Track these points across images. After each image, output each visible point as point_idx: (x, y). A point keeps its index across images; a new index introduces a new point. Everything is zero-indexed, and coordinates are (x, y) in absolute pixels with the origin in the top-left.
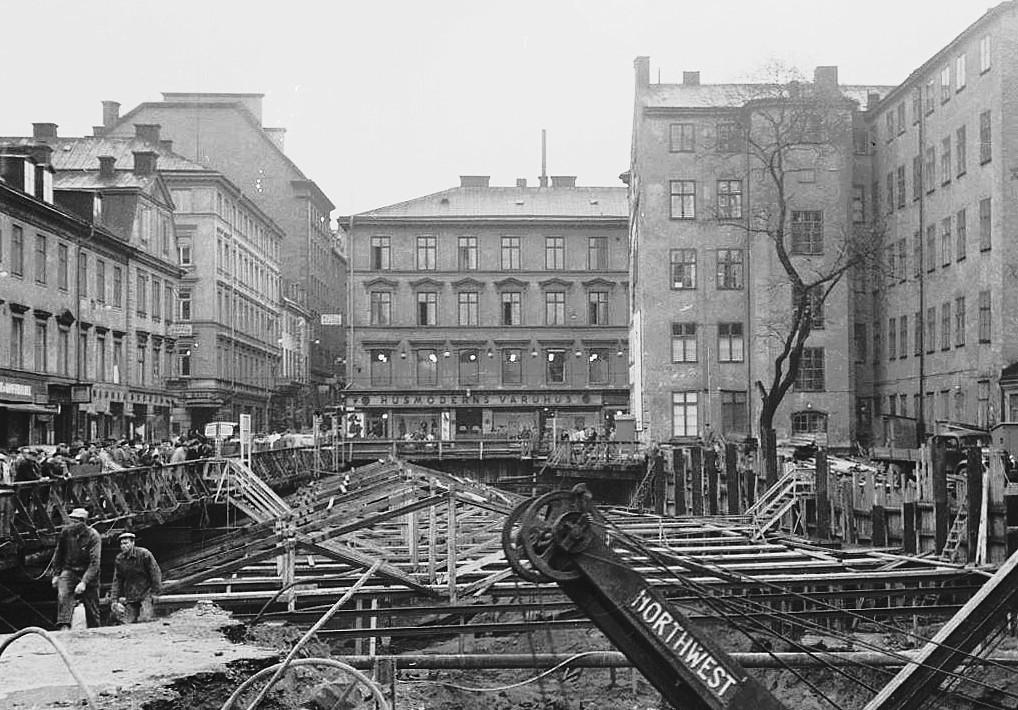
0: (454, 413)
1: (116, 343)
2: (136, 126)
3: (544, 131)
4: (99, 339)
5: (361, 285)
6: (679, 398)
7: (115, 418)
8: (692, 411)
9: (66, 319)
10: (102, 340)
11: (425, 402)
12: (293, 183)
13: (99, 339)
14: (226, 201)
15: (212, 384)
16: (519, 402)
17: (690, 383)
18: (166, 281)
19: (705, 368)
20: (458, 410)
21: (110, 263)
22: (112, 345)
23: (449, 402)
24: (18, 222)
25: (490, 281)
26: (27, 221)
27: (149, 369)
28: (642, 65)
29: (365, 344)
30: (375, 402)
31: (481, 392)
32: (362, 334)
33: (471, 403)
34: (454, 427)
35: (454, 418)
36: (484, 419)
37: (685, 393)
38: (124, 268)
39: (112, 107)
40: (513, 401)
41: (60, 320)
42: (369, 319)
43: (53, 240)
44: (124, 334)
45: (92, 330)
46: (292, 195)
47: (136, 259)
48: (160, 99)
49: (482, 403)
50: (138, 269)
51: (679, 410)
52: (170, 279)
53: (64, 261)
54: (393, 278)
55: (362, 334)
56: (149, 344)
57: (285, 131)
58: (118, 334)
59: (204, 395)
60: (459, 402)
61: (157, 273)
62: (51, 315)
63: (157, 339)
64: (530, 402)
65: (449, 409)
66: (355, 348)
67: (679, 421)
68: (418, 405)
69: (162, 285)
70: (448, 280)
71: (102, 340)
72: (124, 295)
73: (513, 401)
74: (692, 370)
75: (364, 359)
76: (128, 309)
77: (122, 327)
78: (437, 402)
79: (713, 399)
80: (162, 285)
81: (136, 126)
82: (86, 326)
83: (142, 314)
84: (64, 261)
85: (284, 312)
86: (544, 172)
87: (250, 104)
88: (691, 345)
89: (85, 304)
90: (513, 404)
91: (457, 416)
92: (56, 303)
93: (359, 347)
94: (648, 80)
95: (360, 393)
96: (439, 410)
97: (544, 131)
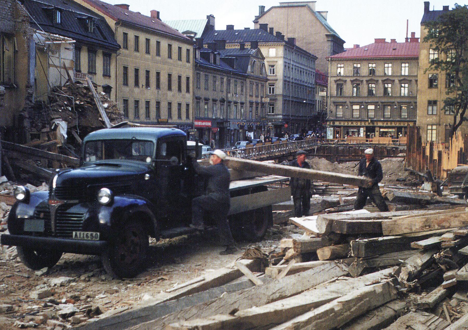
0: (365, 128)
1: (241, 106)
2: (260, 24)
3: (408, 20)
4: (235, 105)
5: (333, 81)
6: (430, 127)
7: (240, 131)
8: (434, 132)
9: (223, 101)
10: (236, 106)
11: (354, 124)
12: (327, 35)
13: (235, 105)
14: (289, 51)
15: (281, 117)
16: (389, 124)
17: (434, 122)
18: (261, 83)
19: (440, 116)
20: (367, 127)
21: (239, 81)
22: (240, 107)
23: (363, 124)
24: (207, 74)
25: (380, 80)
26: (209, 73)
27: (254, 114)
28: (427, 5)
29: (334, 103)
30: (337, 123)
31: (375, 121)
32: (333, 99)
33: (371, 125)
34: (365, 133)
35: (365, 130)
36: (376, 130)
37: (432, 125)
38: (245, 82)
39: (262, 8)
40: (387, 124)
41: (221, 101)
42: (335, 93)
43: (219, 77)
44: (244, 103)
45: (232, 103)
46: (326, 39)
47: (249, 78)
48: (279, 5)
49: (375, 124)
50: (250, 81)
51: (429, 132)
52: (262, 83)
53: (222, 83)
54: (344, 79)
55: (333, 99)
56: (254, 105)
57: (327, 12)
58: (242, 103)
59: (278, 120)
60: (367, 124)
61: (257, 81)
62: (217, 100)
63: (257, 103)
64: (393, 124)
65: (363, 127)
66: (330, 105)
67: (429, 135)
68: (352, 125)
69: (260, 85)
70: (365, 79)
71: (236, 106)
72: (244, 90)
73: (387, 124)
74: (434, 117)
75: (333, 108)
76: (246, 95)
77: (243, 100)
78: (359, 124)
79: (442, 128)
80: (260, 85)
81: (260, 24)
82: (230, 102)
83: (251, 96)
84: (222, 83)
85: (318, 87)
86: (407, 37)
87: (310, 5)
88: (435, 108)
89: (229, 95)
90: (387, 125)
91: (366, 129)
92: (219, 96)
93: (332, 104)
94: (429, 9)
95: (332, 120)
96: (359, 127)
97: (408, 20)
